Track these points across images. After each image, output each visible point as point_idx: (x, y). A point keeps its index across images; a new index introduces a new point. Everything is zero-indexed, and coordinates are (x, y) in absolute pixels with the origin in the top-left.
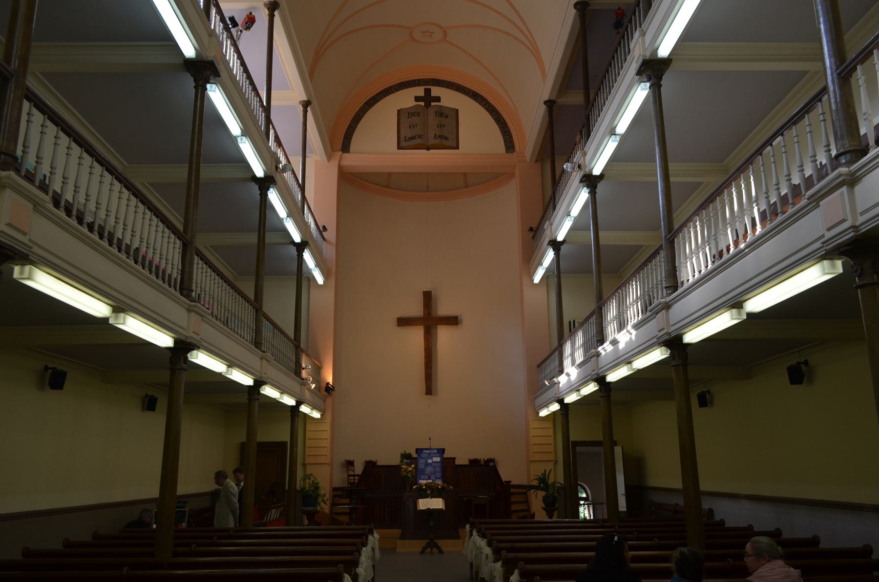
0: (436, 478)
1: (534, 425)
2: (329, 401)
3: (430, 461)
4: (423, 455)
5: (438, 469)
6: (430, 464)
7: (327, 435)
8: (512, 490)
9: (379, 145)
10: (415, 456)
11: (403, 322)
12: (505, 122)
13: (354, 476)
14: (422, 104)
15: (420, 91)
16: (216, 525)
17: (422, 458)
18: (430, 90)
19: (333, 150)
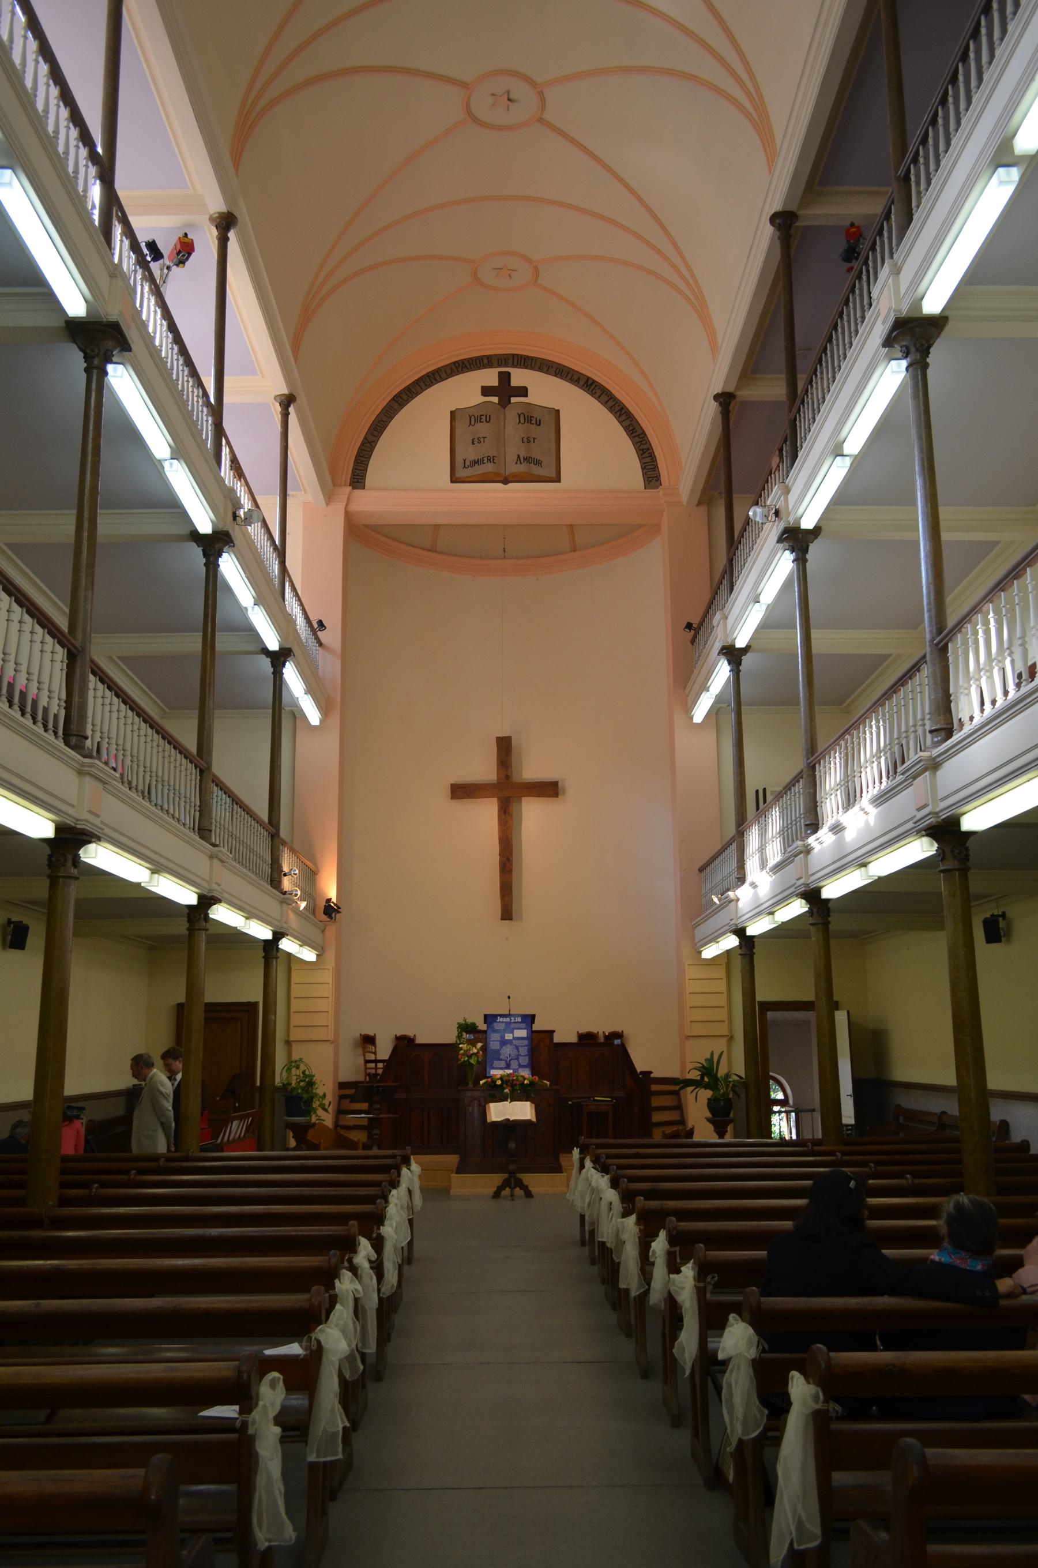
0: (520, 1066)
1: (691, 972)
2: (332, 930)
3: (508, 1036)
4: (496, 1026)
5: (524, 1051)
6: (509, 1042)
7: (327, 991)
8: (654, 1087)
9: (417, 472)
10: (482, 1027)
11: (461, 791)
12: (644, 433)
13: (376, 1061)
14: (495, 399)
15: (490, 377)
16: (135, 1150)
17: (495, 1031)
18: (509, 374)
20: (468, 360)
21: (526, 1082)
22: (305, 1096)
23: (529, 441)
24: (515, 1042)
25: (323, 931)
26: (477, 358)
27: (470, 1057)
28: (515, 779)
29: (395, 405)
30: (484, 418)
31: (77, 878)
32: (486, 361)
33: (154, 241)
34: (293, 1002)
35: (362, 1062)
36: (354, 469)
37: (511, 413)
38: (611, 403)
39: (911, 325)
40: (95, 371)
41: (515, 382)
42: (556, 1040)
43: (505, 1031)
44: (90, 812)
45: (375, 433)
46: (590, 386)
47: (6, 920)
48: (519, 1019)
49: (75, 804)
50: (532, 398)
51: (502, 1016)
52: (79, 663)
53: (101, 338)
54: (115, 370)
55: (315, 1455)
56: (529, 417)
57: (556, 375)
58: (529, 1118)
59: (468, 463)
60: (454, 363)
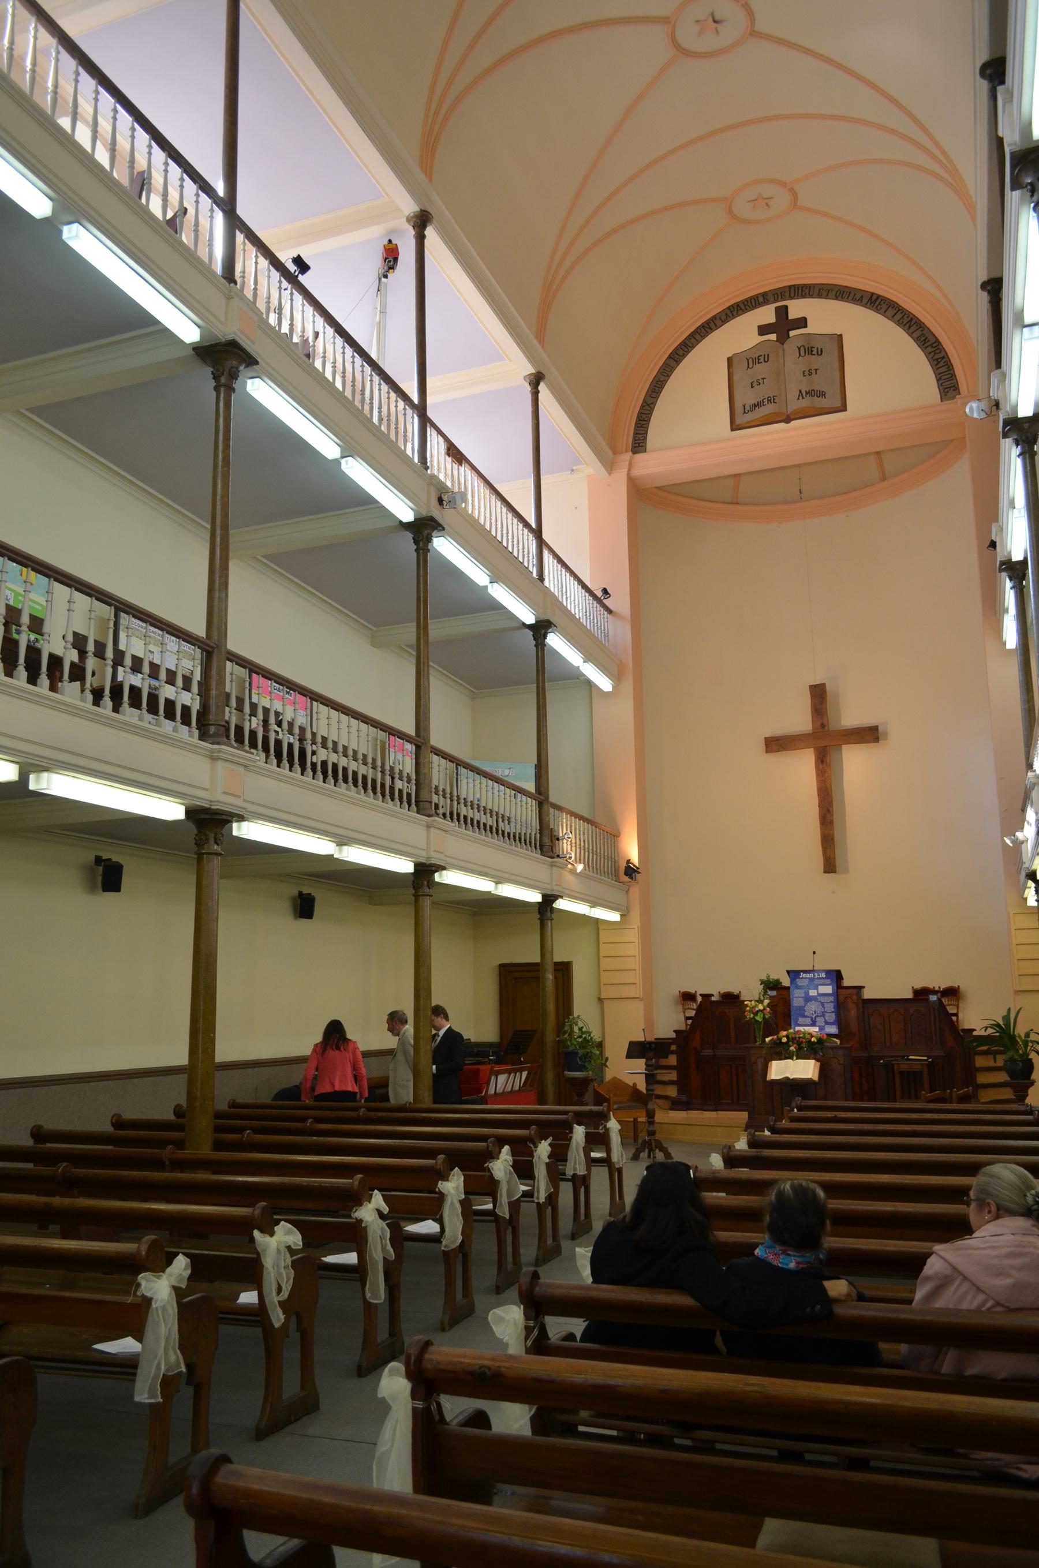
0: (827, 1023)
2: (635, 890)
3: (813, 993)
4: (799, 982)
5: (830, 1007)
6: (814, 999)
7: (634, 949)
9: (697, 428)
10: (786, 982)
11: (776, 744)
12: (937, 341)
14: (773, 337)
15: (767, 314)
16: (393, 1101)
17: (798, 987)
18: (786, 307)
19: (615, 452)
20: (743, 302)
21: (813, 1039)
22: (581, 1052)
23: (810, 374)
24: (820, 999)
25: (627, 892)
26: (752, 298)
27: (756, 1014)
28: (833, 726)
29: (672, 363)
30: (762, 358)
31: (220, 854)
32: (761, 299)
33: (299, 256)
34: (603, 961)
35: (683, 1019)
36: (635, 434)
37: (791, 347)
38: (899, 316)
39: (1032, 157)
40: (222, 389)
41: (793, 315)
42: (866, 997)
43: (809, 987)
44: (225, 793)
45: (654, 395)
46: (875, 302)
47: (297, 893)
48: (823, 975)
49: (207, 787)
50: (812, 328)
51: (805, 972)
52: (215, 658)
53: (224, 358)
54: (253, 384)
55: (146, 1396)
56: (809, 349)
57: (836, 298)
58: (810, 1076)
59: (748, 408)
60: (729, 308)
